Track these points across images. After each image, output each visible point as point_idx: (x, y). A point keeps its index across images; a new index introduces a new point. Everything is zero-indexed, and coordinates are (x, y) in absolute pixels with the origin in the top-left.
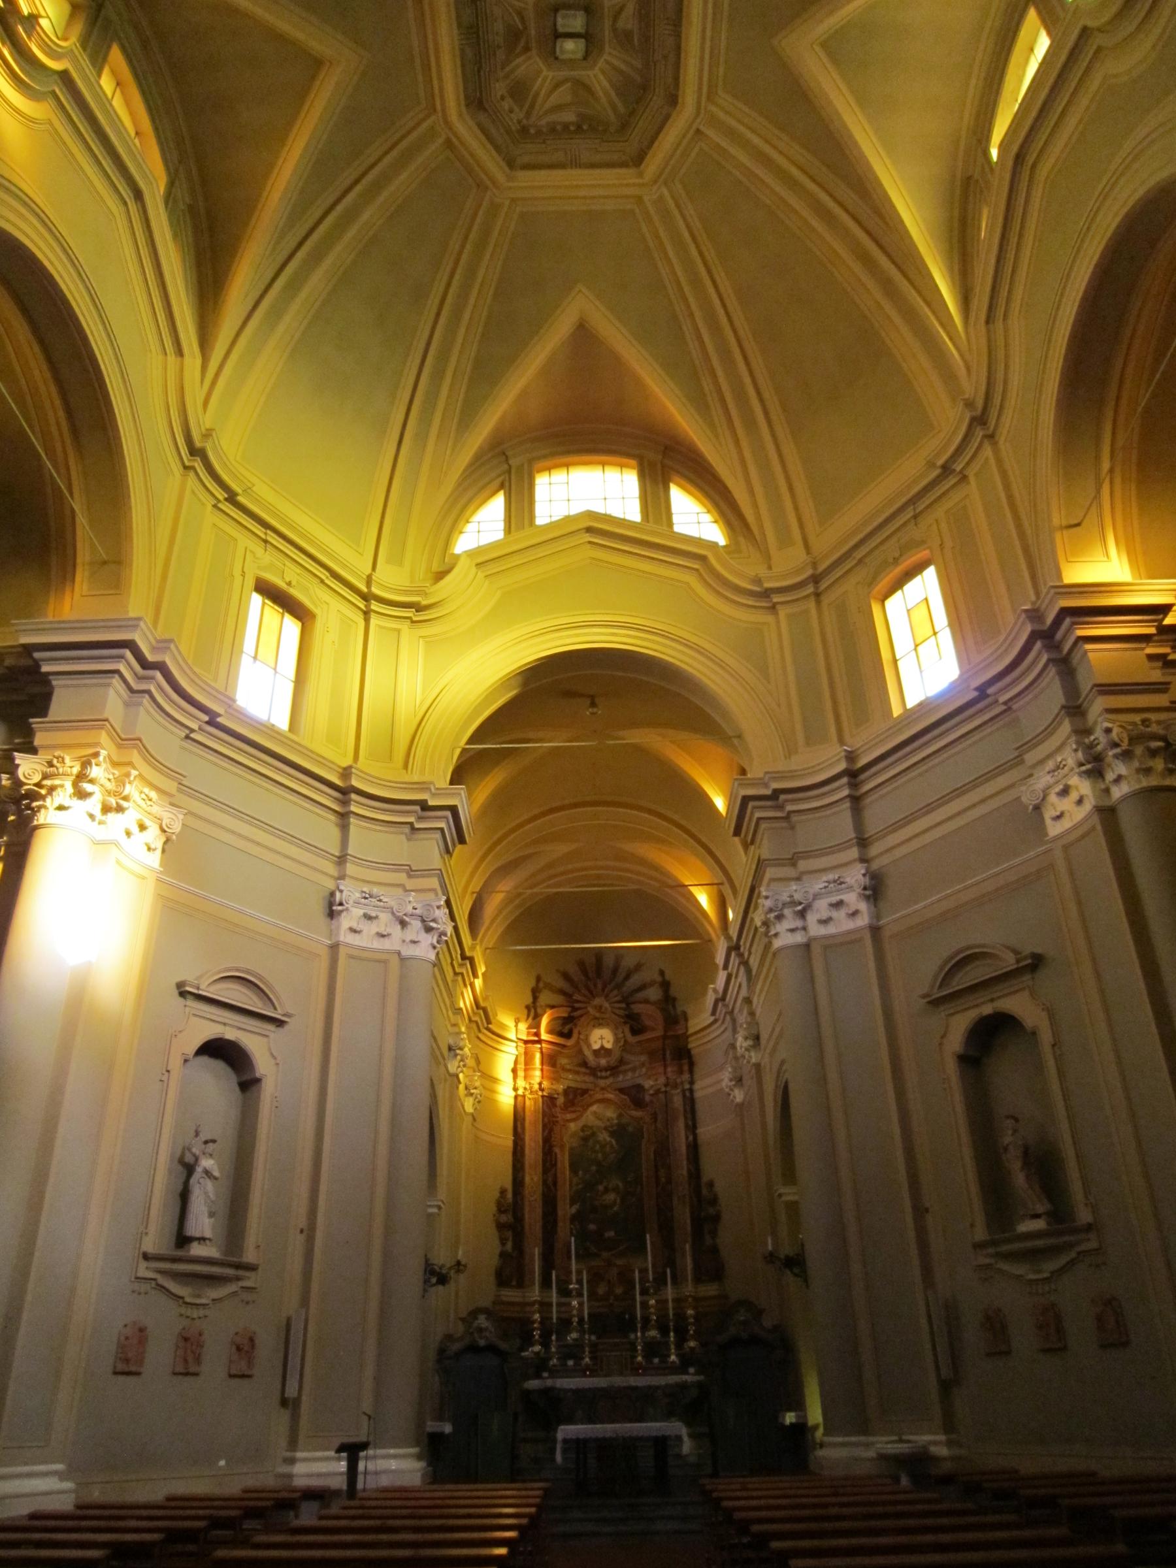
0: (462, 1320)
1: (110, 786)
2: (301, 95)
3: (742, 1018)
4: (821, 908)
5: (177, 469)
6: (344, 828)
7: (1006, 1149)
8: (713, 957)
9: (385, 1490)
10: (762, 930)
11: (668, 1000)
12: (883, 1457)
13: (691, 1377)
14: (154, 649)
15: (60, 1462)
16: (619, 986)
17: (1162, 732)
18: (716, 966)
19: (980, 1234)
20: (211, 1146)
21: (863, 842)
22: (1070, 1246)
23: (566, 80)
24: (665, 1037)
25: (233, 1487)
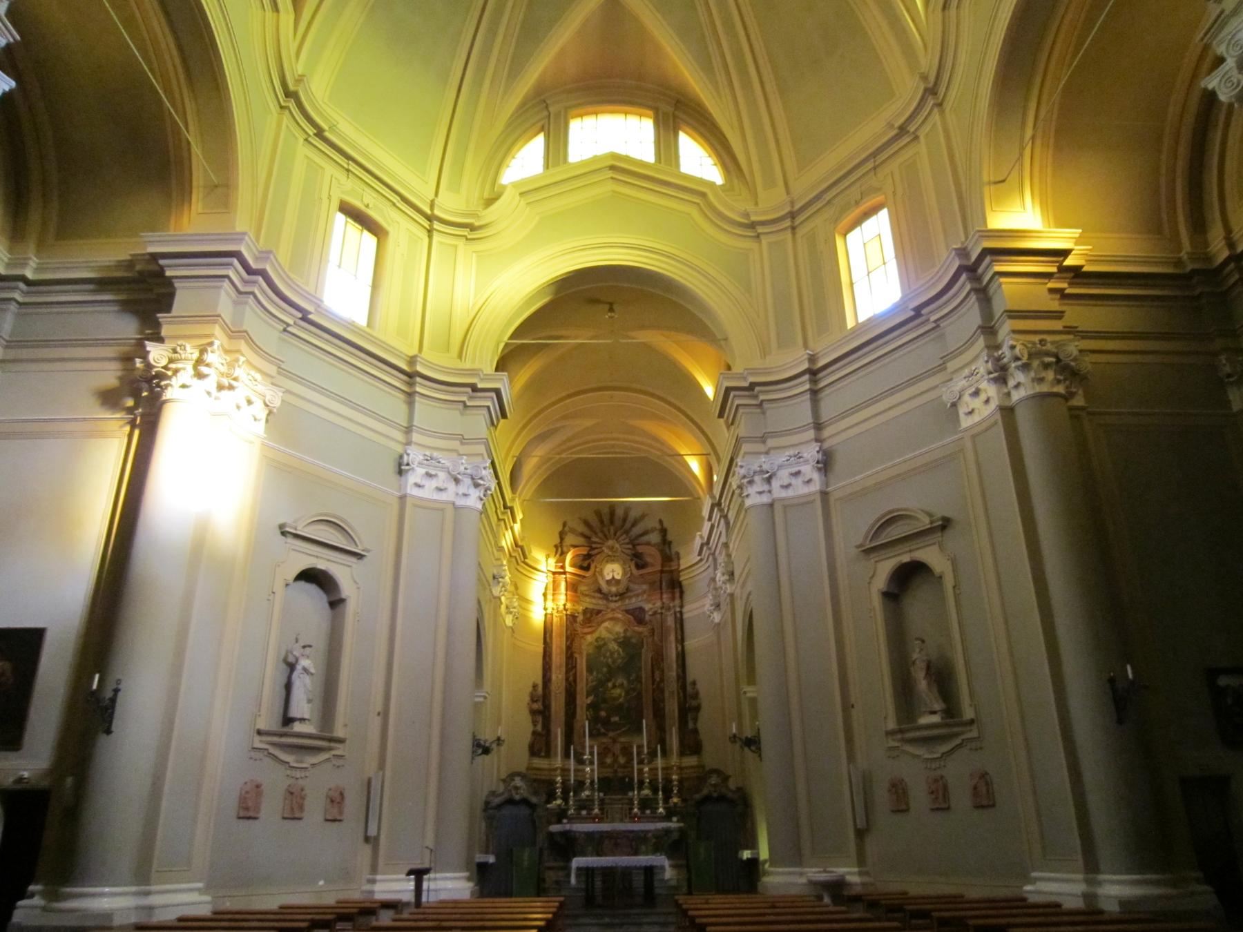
0: (504, 781)
1: (224, 369)
3: (721, 559)
4: (783, 476)
5: (273, 107)
6: (411, 405)
7: (914, 663)
8: (701, 511)
9: (441, 902)
10: (737, 492)
11: (665, 542)
12: (812, 883)
13: (674, 824)
14: (257, 259)
15: (199, 881)
16: (627, 532)
17: (1054, 350)
18: (702, 518)
19: (892, 725)
20: (308, 650)
21: (818, 426)
22: (956, 735)
24: (662, 572)
25: (329, 900)
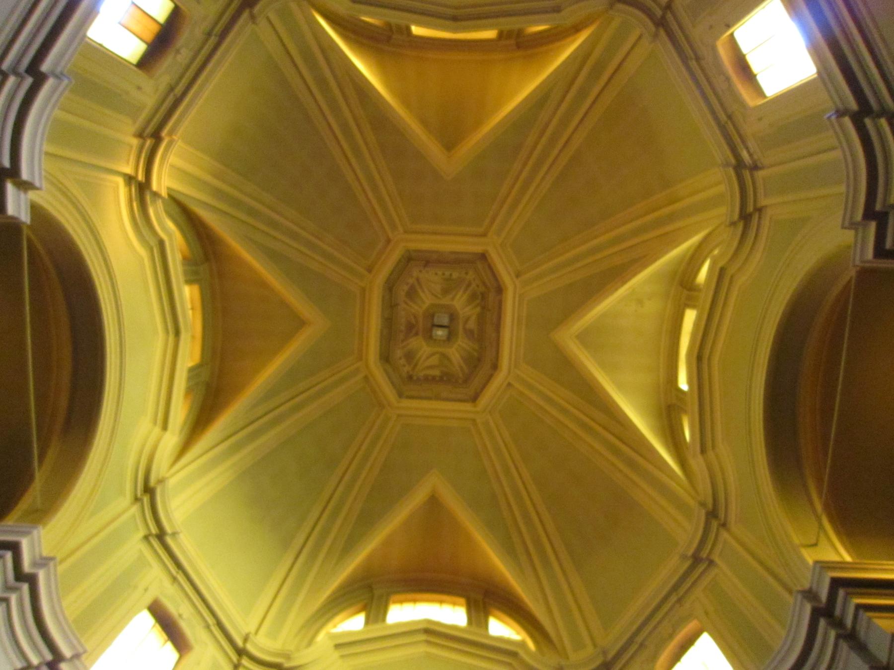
2: (287, 337)
14: (35, 564)
23: (437, 353)
